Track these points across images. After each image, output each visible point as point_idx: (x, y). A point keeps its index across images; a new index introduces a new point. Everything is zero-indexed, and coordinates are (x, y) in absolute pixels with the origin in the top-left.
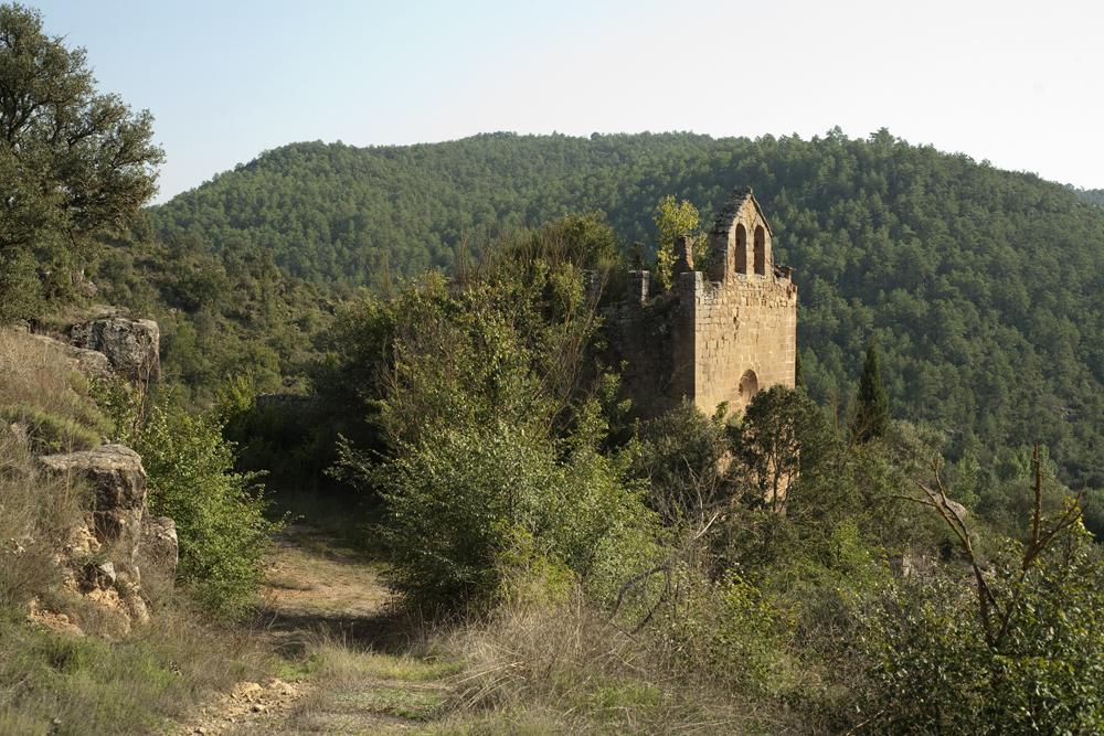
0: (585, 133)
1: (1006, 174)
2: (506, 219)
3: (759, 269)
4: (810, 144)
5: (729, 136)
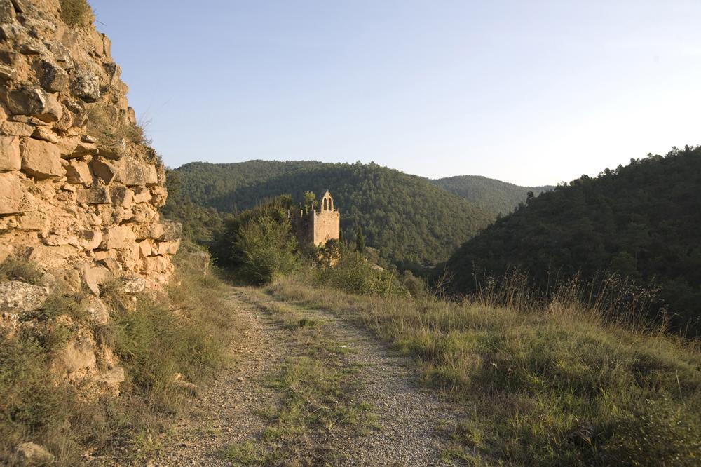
0: (284, 160)
1: (408, 175)
3: (330, 209)
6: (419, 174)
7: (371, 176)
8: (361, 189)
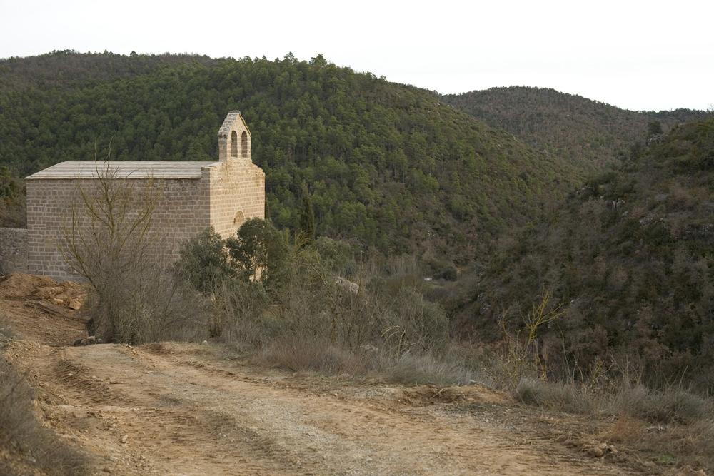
6: (419, 84)
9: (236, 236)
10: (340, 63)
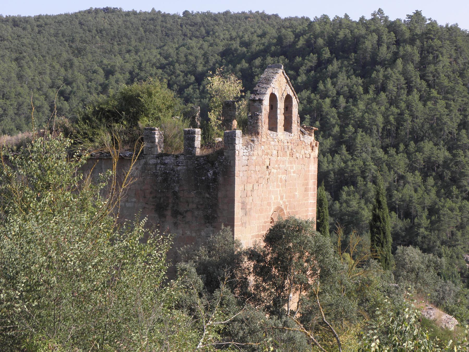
2: (112, 79)
3: (288, 127)
4: (358, 23)
5: (293, 16)
7: (413, 51)
8: (383, 88)
9: (263, 244)
10: (442, 21)
